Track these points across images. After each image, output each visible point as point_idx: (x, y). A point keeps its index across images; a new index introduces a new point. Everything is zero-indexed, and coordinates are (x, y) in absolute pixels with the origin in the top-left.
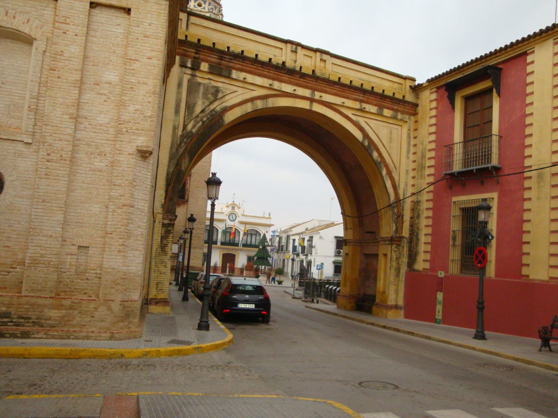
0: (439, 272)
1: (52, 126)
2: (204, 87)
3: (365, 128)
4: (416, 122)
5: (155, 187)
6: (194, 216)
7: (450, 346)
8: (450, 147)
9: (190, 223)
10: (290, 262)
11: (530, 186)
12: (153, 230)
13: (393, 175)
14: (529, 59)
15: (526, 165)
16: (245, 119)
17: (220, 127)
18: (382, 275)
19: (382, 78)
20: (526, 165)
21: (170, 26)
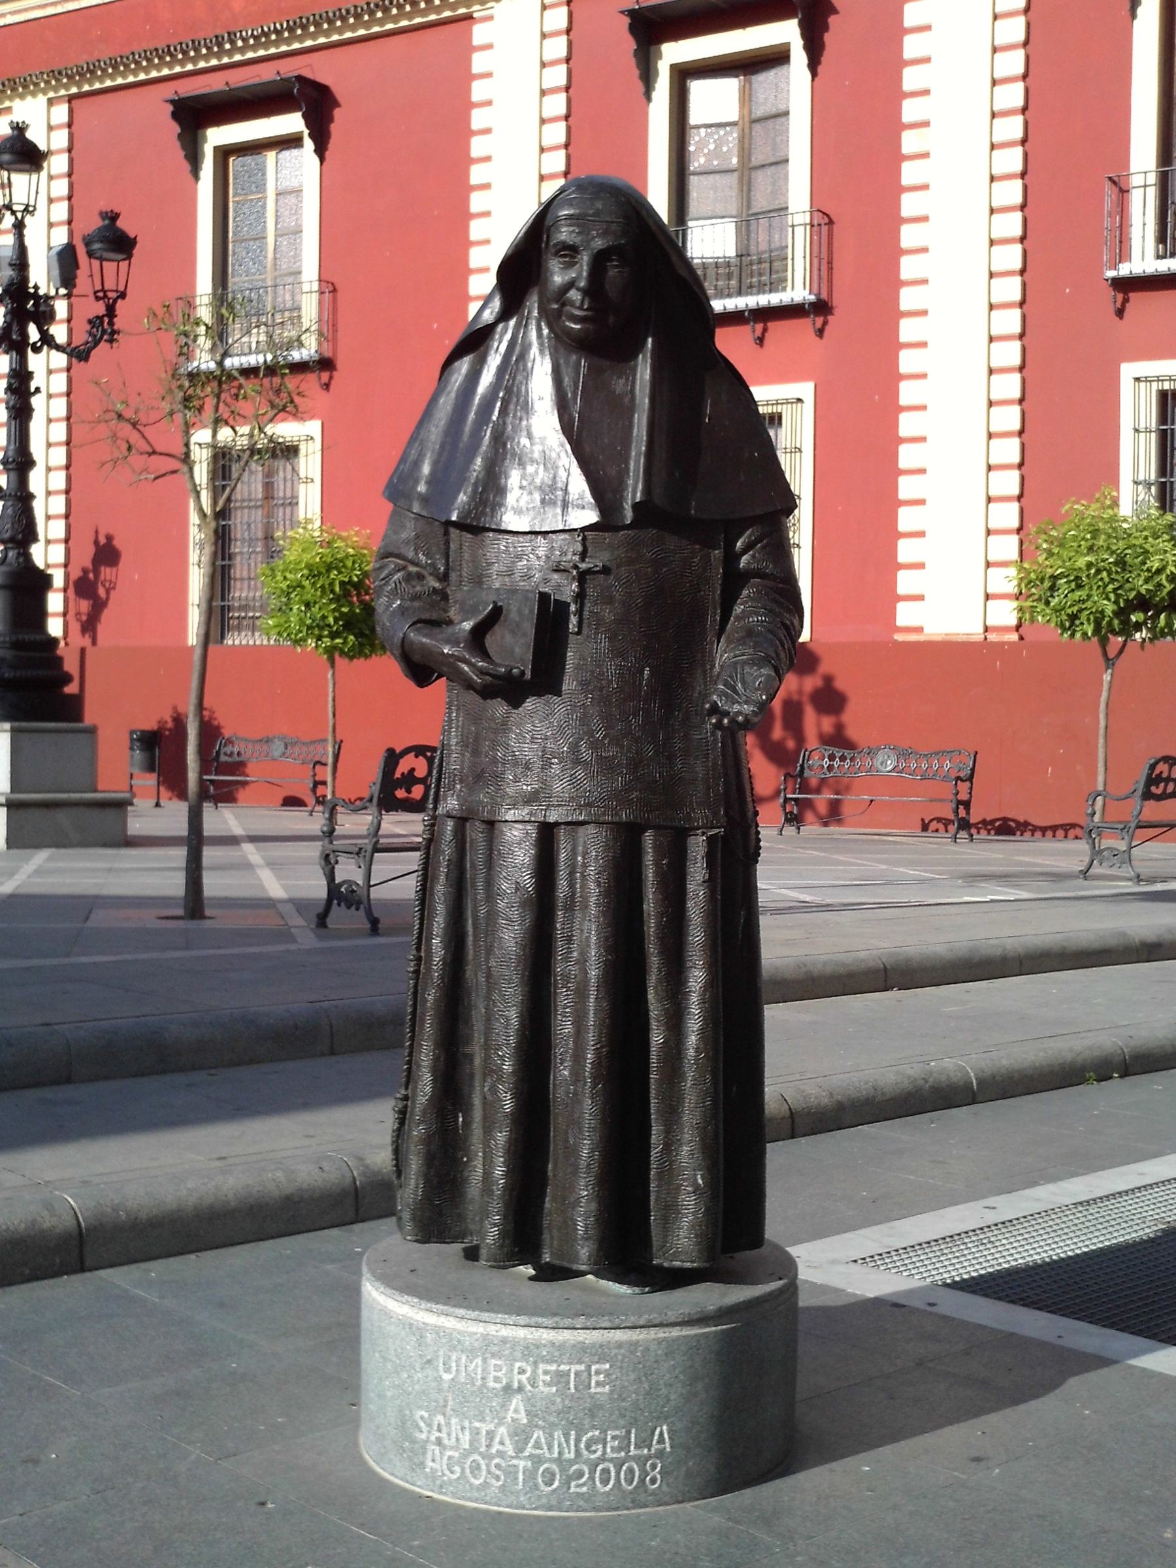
0: (880, 757)
1: (249, 565)
2: (781, 1291)
3: (35, 415)
4: (315, 775)
5: (58, 731)
6: (115, 542)
7: (101, 1023)
8: (561, 1347)
9: (532, 829)
10: (790, 229)
11: (79, 650)
12: (772, 164)
13: (527, 880)
14: (479, 33)
15: (900, 622)
16: (644, 213)
17: (773, 287)
18: (81, 865)
19: (1051, 899)
20: (900, 622)
21: (226, 844)
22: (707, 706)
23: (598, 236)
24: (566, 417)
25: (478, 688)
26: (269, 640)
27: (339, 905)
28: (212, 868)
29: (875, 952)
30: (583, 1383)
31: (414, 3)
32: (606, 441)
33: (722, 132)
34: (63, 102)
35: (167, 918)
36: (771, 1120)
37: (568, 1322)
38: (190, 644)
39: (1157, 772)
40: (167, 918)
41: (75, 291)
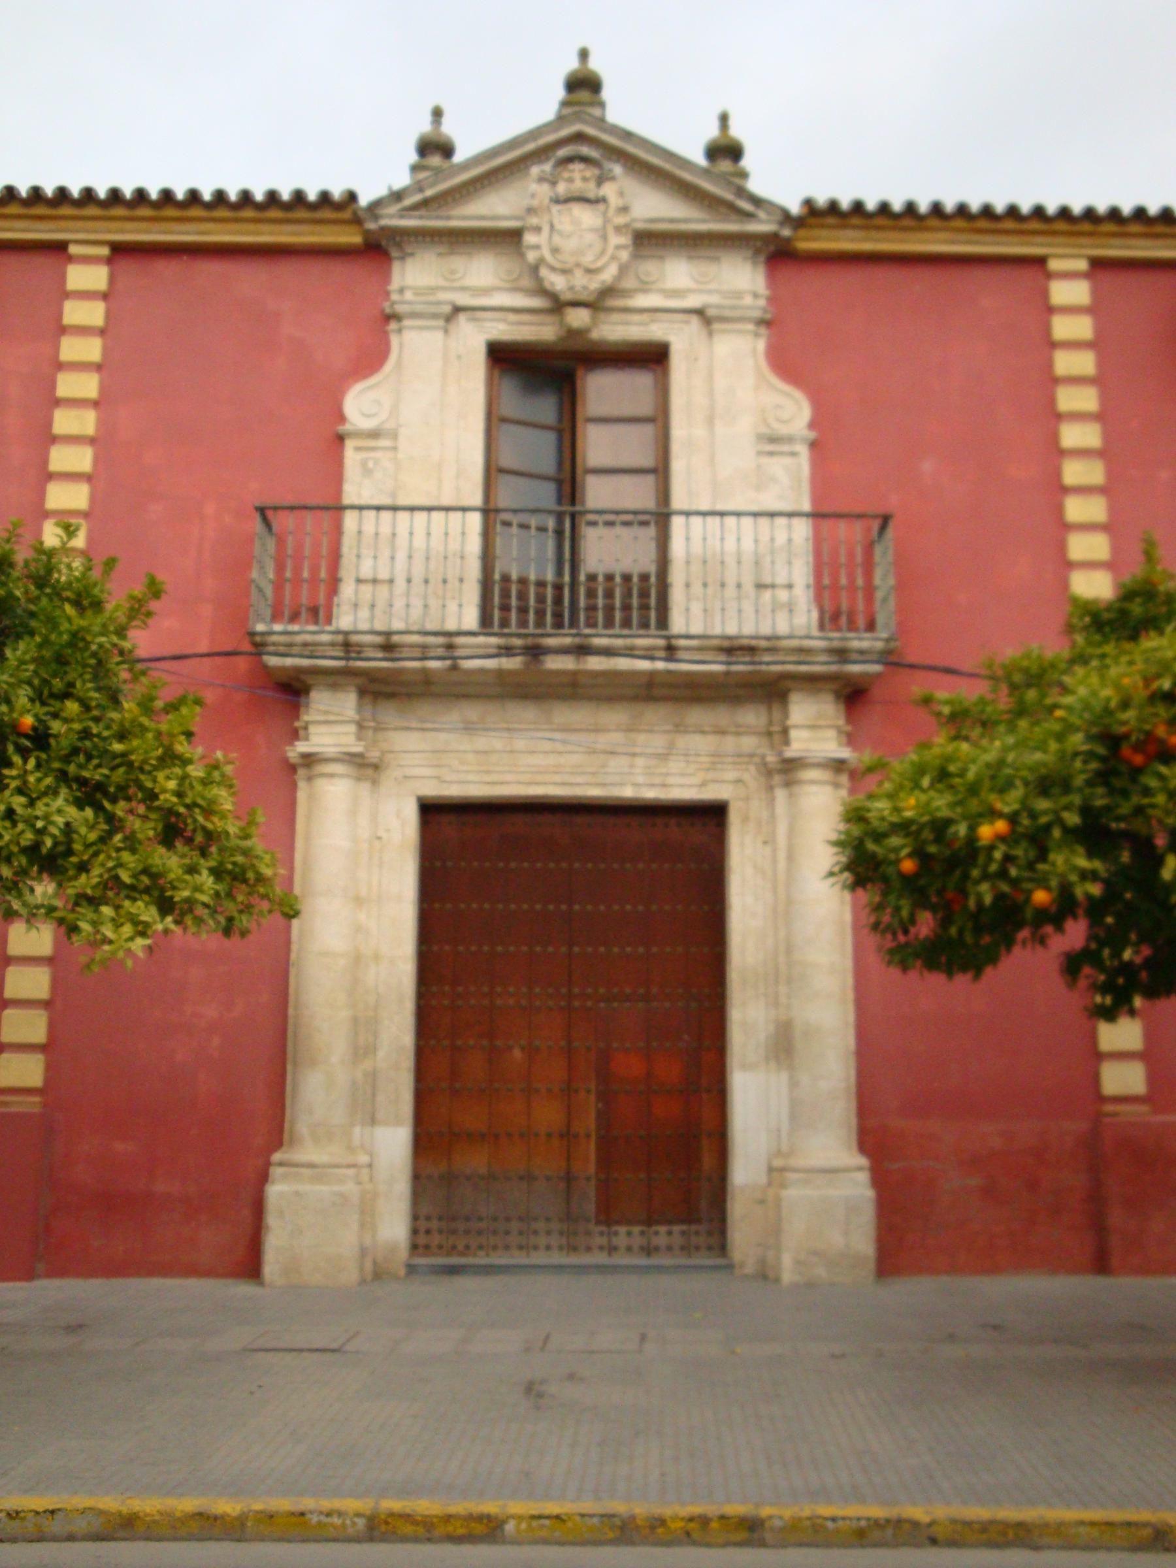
22: (1109, 920)
23: (910, 856)
24: (409, 1529)
25: (789, 683)
26: (23, 832)
27: (1072, 965)
28: (687, 625)
29: (434, 214)
30: (982, 736)
31: (1104, 1198)
32: (235, 755)
33: (557, 1534)
34: (658, 504)
35: (502, 783)
36: (398, 1123)
37: (548, 735)
38: (37, 1110)
39: (121, 845)
40: (502, 783)
41: (242, 664)
